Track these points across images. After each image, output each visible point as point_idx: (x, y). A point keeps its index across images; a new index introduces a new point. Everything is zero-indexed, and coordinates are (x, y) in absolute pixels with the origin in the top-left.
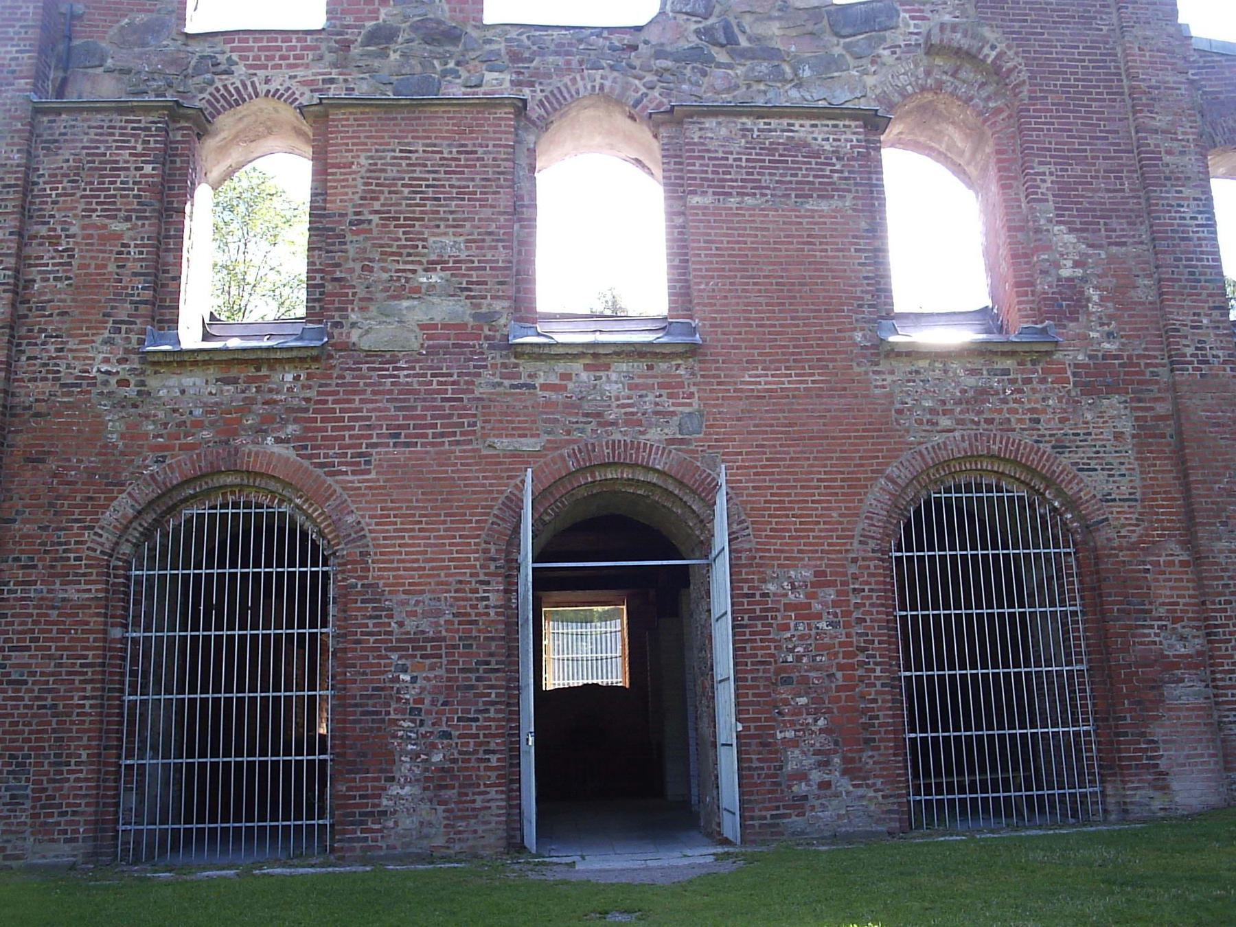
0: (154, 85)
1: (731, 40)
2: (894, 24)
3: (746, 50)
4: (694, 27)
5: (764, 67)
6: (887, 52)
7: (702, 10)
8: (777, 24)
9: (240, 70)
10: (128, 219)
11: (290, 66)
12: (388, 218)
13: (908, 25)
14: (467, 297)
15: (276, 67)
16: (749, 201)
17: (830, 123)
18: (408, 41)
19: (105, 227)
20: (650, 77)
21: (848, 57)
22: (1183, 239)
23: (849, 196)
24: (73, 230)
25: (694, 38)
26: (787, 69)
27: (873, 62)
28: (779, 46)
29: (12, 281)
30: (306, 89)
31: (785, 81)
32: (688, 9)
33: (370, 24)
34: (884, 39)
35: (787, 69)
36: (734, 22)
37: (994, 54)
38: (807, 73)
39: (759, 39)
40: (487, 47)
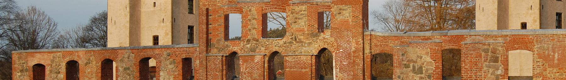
0: (221, 50)
1: (296, 40)
2: (320, 35)
3: (298, 41)
4: (291, 37)
5: (300, 44)
6: (319, 41)
7: (291, 35)
8: (302, 36)
9: (231, 47)
10: (218, 72)
11: (237, 46)
12: (248, 73)
13: (322, 35)
14: (256, 30)
15: (236, 46)
16: (294, 70)
17: (306, 56)
18: (252, 42)
19: (216, 73)
20: (283, 48)
21: (313, 42)
22: (357, 76)
23: (308, 69)
24: (213, 74)
25: (290, 39)
26: (304, 44)
27: (316, 43)
28: (303, 40)
29: (441, 70)
30: (239, 50)
31: (303, 46)
32: (289, 35)
33: (247, 39)
34: (319, 38)
35: (304, 44)
36: (296, 36)
37: (332, 43)
38: (306, 45)
39: (300, 39)
40: (262, 43)
